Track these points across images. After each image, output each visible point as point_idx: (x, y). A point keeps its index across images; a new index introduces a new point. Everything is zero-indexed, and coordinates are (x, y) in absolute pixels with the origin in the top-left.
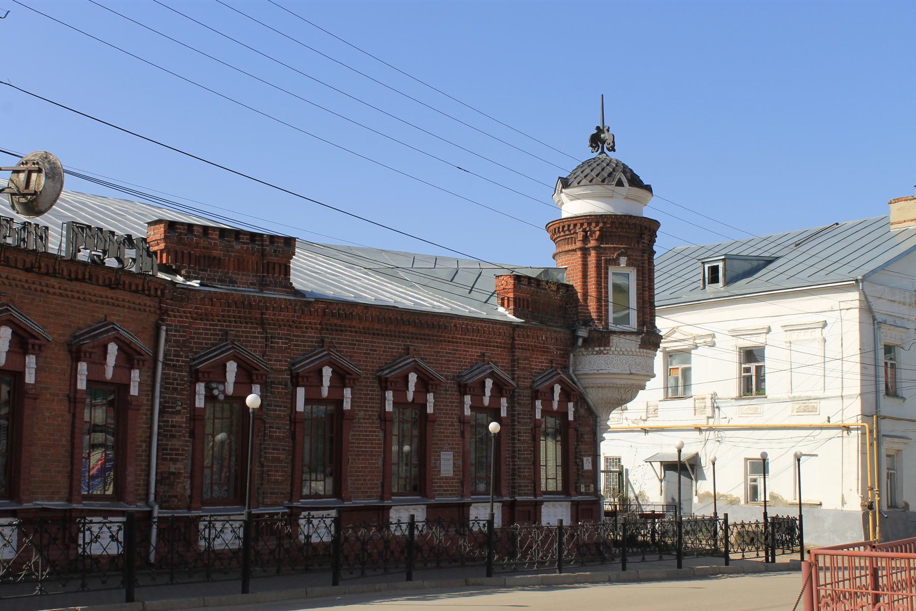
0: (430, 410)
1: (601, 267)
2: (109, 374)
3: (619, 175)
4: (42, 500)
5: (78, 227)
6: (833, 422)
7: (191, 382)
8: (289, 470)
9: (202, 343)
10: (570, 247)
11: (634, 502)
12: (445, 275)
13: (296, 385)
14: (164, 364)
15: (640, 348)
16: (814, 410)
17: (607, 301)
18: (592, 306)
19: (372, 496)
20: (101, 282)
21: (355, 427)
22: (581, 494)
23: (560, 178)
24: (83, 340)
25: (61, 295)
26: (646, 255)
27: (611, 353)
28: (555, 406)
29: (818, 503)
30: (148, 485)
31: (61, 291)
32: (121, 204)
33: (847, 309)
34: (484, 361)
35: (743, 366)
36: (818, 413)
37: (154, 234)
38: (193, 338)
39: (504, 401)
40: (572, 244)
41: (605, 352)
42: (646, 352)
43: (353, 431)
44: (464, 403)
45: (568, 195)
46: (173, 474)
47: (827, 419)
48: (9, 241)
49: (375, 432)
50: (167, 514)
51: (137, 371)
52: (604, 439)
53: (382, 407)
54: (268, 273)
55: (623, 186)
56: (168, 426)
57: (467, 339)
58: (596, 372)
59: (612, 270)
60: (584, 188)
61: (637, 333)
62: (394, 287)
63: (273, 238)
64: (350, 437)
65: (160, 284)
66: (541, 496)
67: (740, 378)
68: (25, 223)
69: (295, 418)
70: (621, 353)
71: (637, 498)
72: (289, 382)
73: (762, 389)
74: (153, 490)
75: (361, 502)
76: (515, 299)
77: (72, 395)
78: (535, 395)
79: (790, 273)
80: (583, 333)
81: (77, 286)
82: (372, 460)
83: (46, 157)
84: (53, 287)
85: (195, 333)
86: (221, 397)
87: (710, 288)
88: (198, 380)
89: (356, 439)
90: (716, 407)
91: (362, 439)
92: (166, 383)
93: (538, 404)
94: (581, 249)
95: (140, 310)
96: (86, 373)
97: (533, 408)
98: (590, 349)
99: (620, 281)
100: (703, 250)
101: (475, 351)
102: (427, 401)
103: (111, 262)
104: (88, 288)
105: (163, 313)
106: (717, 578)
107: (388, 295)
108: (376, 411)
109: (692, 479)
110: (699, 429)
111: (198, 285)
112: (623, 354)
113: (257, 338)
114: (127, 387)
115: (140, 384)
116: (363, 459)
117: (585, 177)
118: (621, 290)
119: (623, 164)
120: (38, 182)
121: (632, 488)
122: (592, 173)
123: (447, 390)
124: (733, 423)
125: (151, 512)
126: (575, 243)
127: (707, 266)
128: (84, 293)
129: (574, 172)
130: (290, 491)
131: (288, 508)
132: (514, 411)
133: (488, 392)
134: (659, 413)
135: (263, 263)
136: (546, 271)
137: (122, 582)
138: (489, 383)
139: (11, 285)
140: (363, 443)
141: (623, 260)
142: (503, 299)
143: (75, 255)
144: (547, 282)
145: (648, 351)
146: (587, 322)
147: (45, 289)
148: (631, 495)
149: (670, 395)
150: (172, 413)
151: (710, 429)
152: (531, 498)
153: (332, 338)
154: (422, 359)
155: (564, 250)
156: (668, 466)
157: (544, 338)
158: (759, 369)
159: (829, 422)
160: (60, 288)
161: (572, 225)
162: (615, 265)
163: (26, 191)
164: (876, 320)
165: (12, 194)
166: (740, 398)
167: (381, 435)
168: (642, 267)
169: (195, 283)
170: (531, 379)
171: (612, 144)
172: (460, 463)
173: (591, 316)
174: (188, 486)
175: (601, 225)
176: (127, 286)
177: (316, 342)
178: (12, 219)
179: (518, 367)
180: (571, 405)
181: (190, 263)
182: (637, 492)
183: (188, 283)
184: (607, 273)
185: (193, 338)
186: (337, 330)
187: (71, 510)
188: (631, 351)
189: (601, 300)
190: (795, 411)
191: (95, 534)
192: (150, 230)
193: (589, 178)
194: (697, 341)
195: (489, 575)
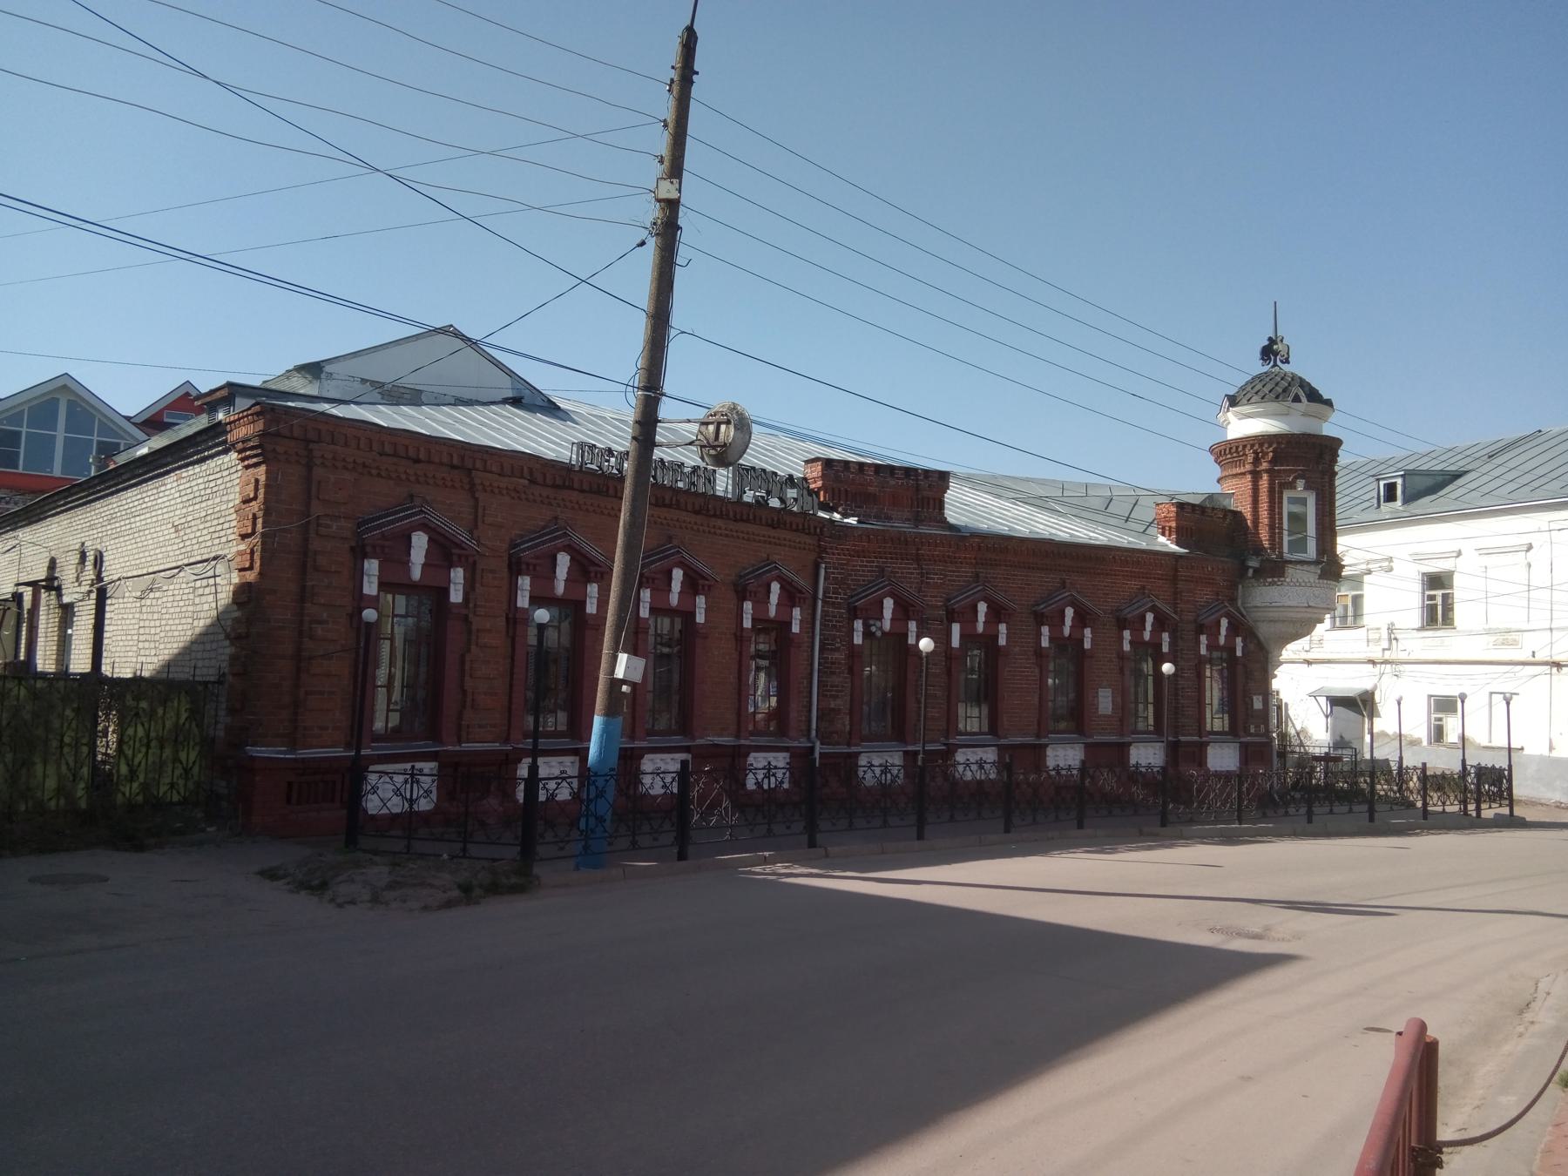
0: (1087, 645)
1: (1275, 491)
2: (772, 612)
3: (1295, 390)
4: (713, 736)
5: (743, 469)
6: (1538, 658)
7: (849, 619)
9: (859, 580)
10: (1238, 470)
11: (1295, 742)
12: (1098, 504)
13: (951, 620)
14: (823, 601)
15: (1319, 579)
16: (1515, 643)
17: (1281, 528)
18: (1264, 534)
20: (764, 522)
22: (1251, 735)
23: (1226, 395)
24: (748, 580)
25: (727, 536)
26: (1327, 478)
27: (1286, 584)
28: (1222, 640)
29: (1520, 747)
30: (809, 721)
31: (727, 532)
32: (768, 439)
34: (1144, 593)
35: (1427, 593)
36: (1520, 646)
37: (812, 472)
38: (851, 575)
39: (1166, 636)
40: (1240, 466)
41: (1279, 583)
42: (1323, 583)
44: (1123, 638)
45: (1236, 414)
46: (833, 709)
47: (1531, 654)
48: (680, 485)
50: (829, 749)
51: (798, 609)
52: (1275, 676)
54: (923, 509)
55: (1300, 401)
56: (827, 663)
57: (1127, 571)
59: (1287, 494)
61: (1316, 563)
62: (1045, 517)
63: (927, 473)
65: (819, 522)
66: (1206, 736)
67: (1423, 607)
68: (694, 466)
70: (1298, 584)
71: (1298, 734)
73: (1448, 619)
74: (814, 726)
75: (1019, 740)
76: (1177, 527)
77: (738, 634)
78: (1200, 629)
79: (1486, 489)
80: (1253, 563)
81: (742, 526)
83: (734, 408)
84: (720, 528)
85: (852, 570)
86: (879, 634)
87: (1386, 508)
88: (856, 617)
90: (1392, 639)
92: (826, 620)
93: (1203, 638)
94: (1250, 472)
95: (800, 548)
96: (751, 612)
97: (1198, 642)
99: (1296, 509)
100: (1374, 464)
101: (1134, 584)
103: (774, 503)
104: (751, 528)
105: (822, 551)
106: (1417, 834)
107: (1042, 527)
108: (1032, 647)
109: (1364, 716)
110: (1373, 662)
111: (855, 523)
112: (1300, 585)
113: (912, 573)
114: (789, 624)
115: (801, 621)
117: (1256, 393)
118: (1298, 520)
119: (1300, 378)
120: (728, 433)
121: (1293, 723)
122: (1264, 389)
123: (1105, 625)
124: (1413, 657)
125: (812, 749)
126: (1244, 466)
127: (1382, 483)
128: (748, 533)
129: (1242, 388)
131: (945, 744)
133: (1149, 627)
134: (1325, 644)
135: (918, 499)
136: (1211, 497)
137: (805, 827)
138: (1150, 617)
139: (681, 527)
141: (1300, 484)
142: (1163, 528)
143: (741, 496)
144: (1213, 509)
145: (1329, 582)
146: (1258, 550)
147: (713, 530)
148: (1292, 731)
149: (1338, 624)
150: (832, 649)
151: (1386, 662)
152: (1196, 738)
153: (986, 573)
154: (1078, 592)
155: (1231, 473)
156: (1335, 701)
157: (1209, 569)
158: (1447, 599)
159: (1534, 656)
160: (726, 529)
163: (716, 443)
165: (702, 447)
166: (1422, 629)
167: (1037, 671)
168: (1322, 490)
169: (852, 521)
170: (1195, 612)
171: (1286, 356)
172: (1119, 699)
173: (1263, 545)
174: (847, 722)
176: (788, 525)
178: (683, 464)
179: (1181, 600)
180: (1239, 640)
181: (847, 501)
182: (1299, 728)
183: (846, 520)
184: (1281, 498)
185: (851, 575)
186: (991, 565)
187: (739, 746)
188: (1309, 582)
189: (1274, 527)
190: (1491, 644)
191: (779, 780)
192: (807, 468)
193: (1261, 394)
194: (1370, 566)
195: (1163, 825)
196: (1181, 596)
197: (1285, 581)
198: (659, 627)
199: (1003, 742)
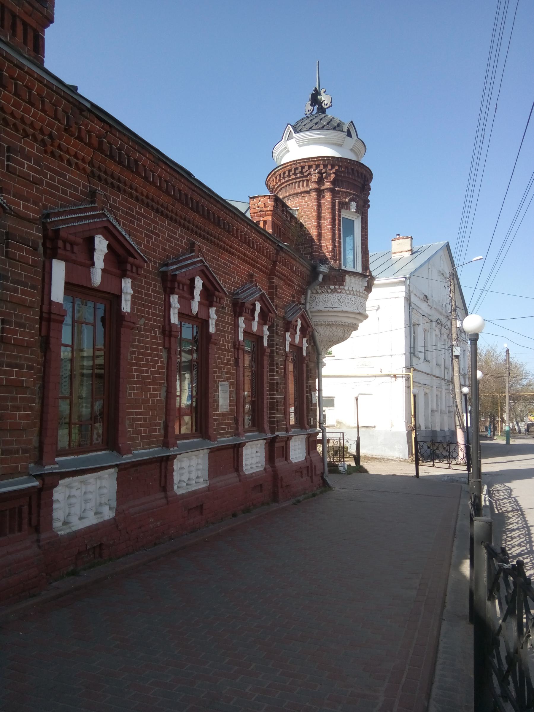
8: (36, 406)
19: (152, 443)
21: (134, 340)
27: (344, 292)
29: (374, 426)
33: (395, 298)
41: (339, 291)
43: (132, 346)
49: (157, 350)
53: (167, 315)
58: (331, 309)
60: (319, 132)
64: (129, 356)
69: (50, 313)
72: (41, 242)
82: (154, 390)
89: (136, 359)
91: (142, 360)
98: (326, 287)
102: (209, 317)
108: (159, 322)
112: (353, 294)
116: (143, 389)
130: (37, 445)
131: (37, 477)
132: (273, 341)
140: (144, 365)
146: (324, 261)
161: (307, 168)
162: (347, 209)
164: (411, 306)
167: (164, 355)
172: (234, 396)
175: (336, 168)
177: (82, 192)
196: (276, 291)
197: (344, 289)
198: (235, 452)
199: (127, 458)
